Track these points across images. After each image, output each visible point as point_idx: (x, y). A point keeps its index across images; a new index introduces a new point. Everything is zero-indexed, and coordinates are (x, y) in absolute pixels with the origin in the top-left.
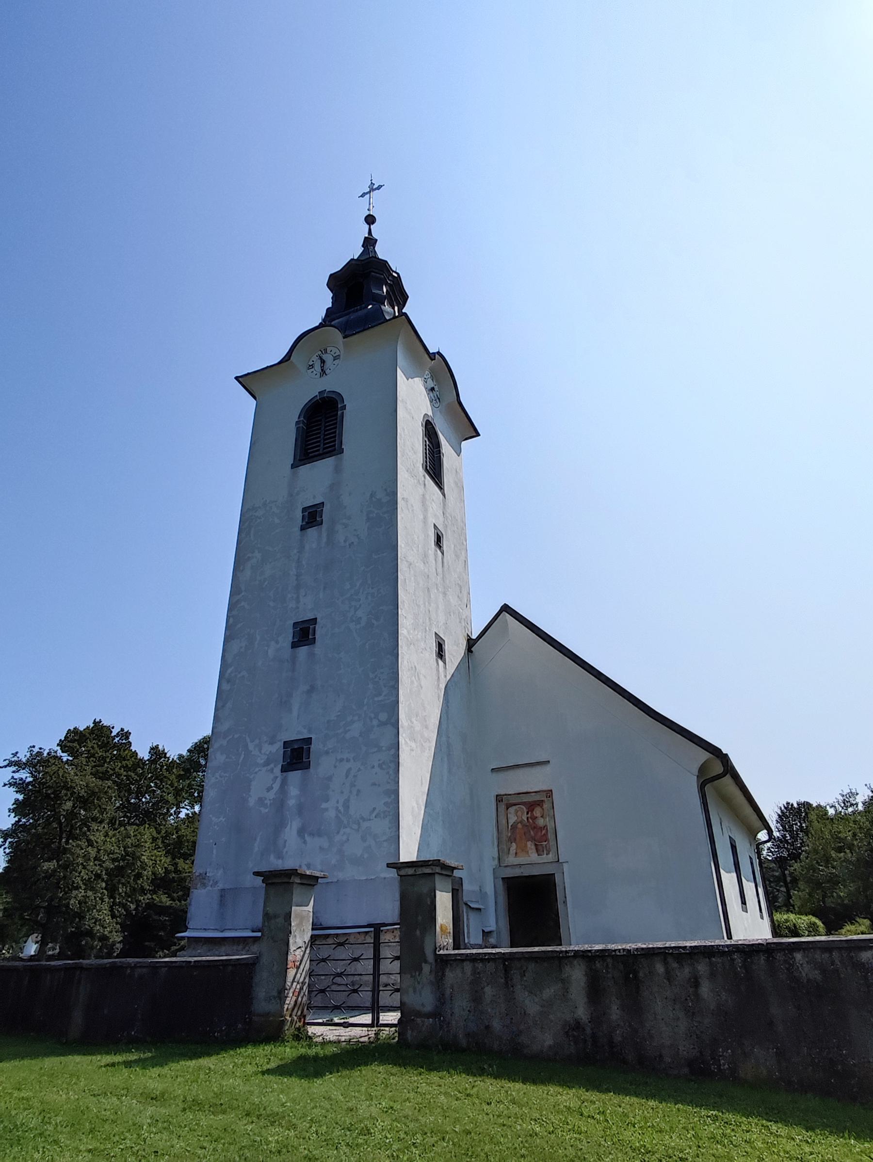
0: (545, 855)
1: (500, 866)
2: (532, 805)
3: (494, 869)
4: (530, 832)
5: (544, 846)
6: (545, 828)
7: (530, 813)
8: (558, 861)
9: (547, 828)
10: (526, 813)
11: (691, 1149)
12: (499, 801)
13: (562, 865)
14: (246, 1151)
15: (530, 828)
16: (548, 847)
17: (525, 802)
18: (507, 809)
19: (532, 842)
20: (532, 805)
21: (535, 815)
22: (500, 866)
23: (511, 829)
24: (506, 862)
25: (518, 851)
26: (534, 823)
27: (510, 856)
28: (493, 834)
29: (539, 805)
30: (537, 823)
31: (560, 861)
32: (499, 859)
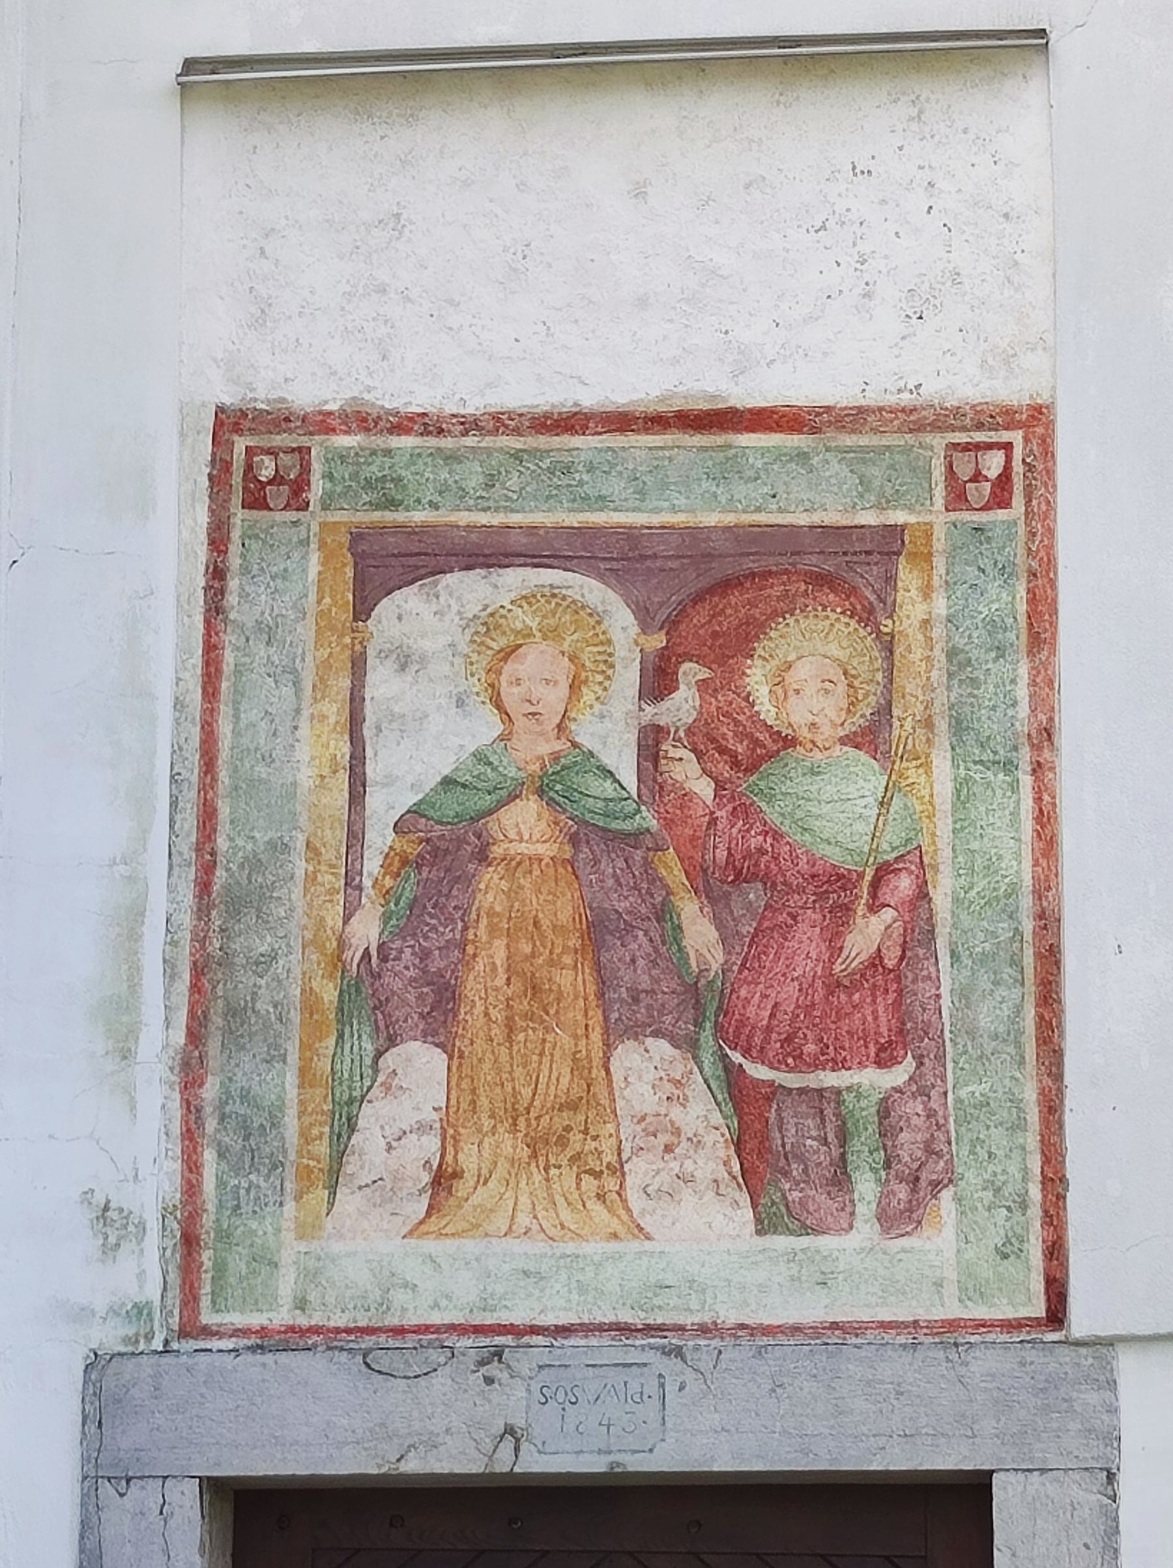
0: (866, 1229)
1: (190, 1329)
2: (725, 586)
3: (96, 1364)
4: (664, 913)
5: (868, 1110)
6: (904, 884)
7: (691, 672)
8: (1056, 1316)
9: (922, 895)
10: (628, 678)
11: (450, 1301)
12: (256, 500)
13: (1107, 1367)
14: (969, 974)
15: (672, 869)
16: (909, 1143)
17: (631, 535)
18: (363, 609)
19: (691, 1045)
20: (725, 586)
21: (766, 709)
22: (190, 1329)
23: (396, 863)
24: (286, 1285)
25: (469, 1159)
26: (744, 811)
27: (348, 1201)
28: (138, 913)
29: (821, 580)
30: (772, 814)
31: (1080, 1322)
32: (190, 1241)
